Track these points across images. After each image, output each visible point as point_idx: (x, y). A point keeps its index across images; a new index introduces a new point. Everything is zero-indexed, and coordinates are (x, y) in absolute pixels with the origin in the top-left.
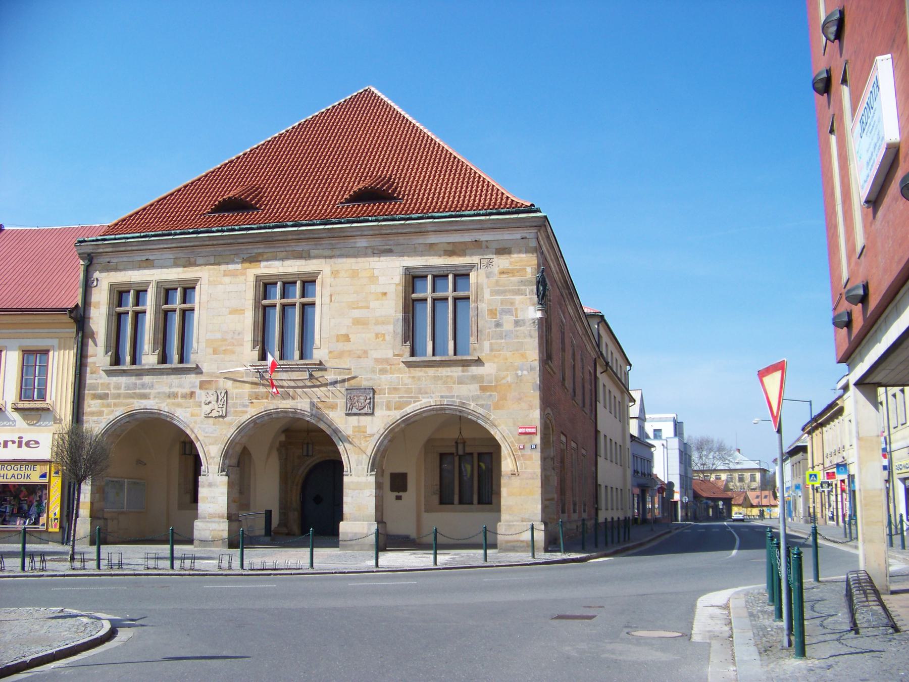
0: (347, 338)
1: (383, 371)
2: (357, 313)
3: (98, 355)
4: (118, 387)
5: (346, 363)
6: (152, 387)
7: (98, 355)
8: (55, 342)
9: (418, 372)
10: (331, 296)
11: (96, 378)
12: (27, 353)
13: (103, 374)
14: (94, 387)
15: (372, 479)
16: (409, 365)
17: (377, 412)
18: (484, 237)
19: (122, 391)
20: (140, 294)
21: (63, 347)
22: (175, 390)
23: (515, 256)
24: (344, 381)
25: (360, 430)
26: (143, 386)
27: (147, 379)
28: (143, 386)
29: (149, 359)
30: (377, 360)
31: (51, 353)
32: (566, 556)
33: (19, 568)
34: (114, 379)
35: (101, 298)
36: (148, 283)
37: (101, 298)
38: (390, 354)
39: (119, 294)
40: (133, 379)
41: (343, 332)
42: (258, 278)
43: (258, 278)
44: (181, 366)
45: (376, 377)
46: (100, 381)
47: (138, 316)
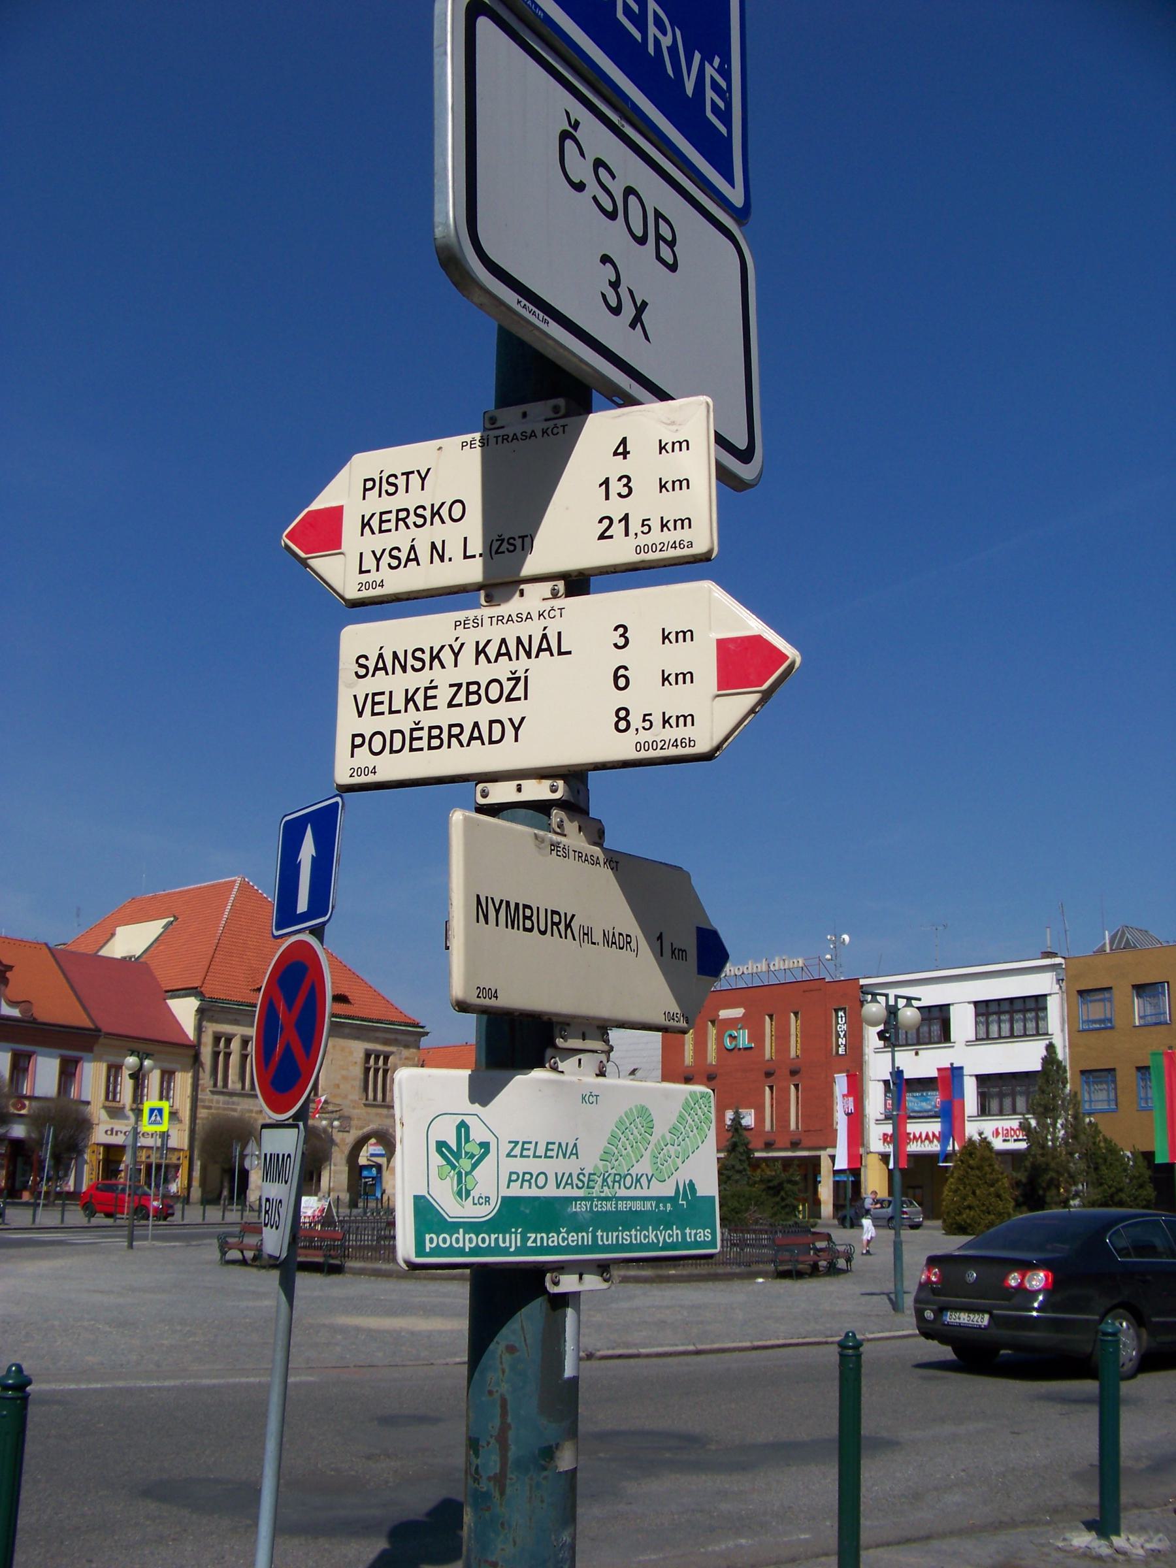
0: (338, 1086)
1: (354, 1108)
2: (344, 1072)
3: (206, 1079)
4: (218, 1102)
5: (338, 1101)
6: (238, 1104)
7: (206, 1079)
8: (179, 1066)
9: (370, 1110)
10: (332, 1061)
11: (205, 1095)
12: (163, 1073)
13: (209, 1093)
14: (203, 1101)
15: (347, 1168)
16: (366, 1105)
17: (352, 1131)
18: (400, 1037)
19: (221, 1105)
20: (228, 1041)
21: (184, 1070)
22: (251, 1108)
23: (411, 1050)
24: (337, 1111)
25: (343, 1140)
26: (233, 1103)
27: (235, 1099)
28: (233, 1103)
29: (233, 1083)
30: (352, 1101)
31: (176, 1073)
32: (1155, 1212)
33: (180, 1219)
34: (216, 1097)
35: (207, 1039)
36: (234, 1035)
37: (207, 1039)
38: (357, 1098)
39: (217, 1038)
40: (227, 1098)
41: (337, 1082)
42: (214, 1033)
43: (214, 1033)
44: (374, 1103)
45: (351, 1110)
46: (207, 1097)
47: (228, 1055)
